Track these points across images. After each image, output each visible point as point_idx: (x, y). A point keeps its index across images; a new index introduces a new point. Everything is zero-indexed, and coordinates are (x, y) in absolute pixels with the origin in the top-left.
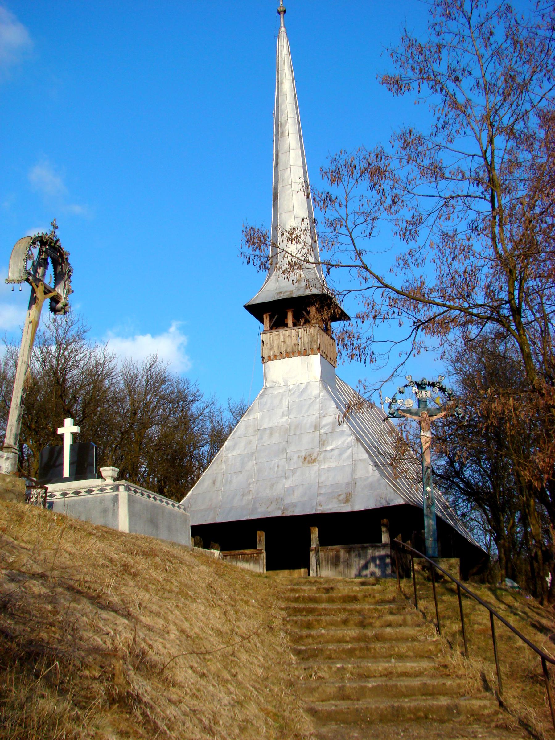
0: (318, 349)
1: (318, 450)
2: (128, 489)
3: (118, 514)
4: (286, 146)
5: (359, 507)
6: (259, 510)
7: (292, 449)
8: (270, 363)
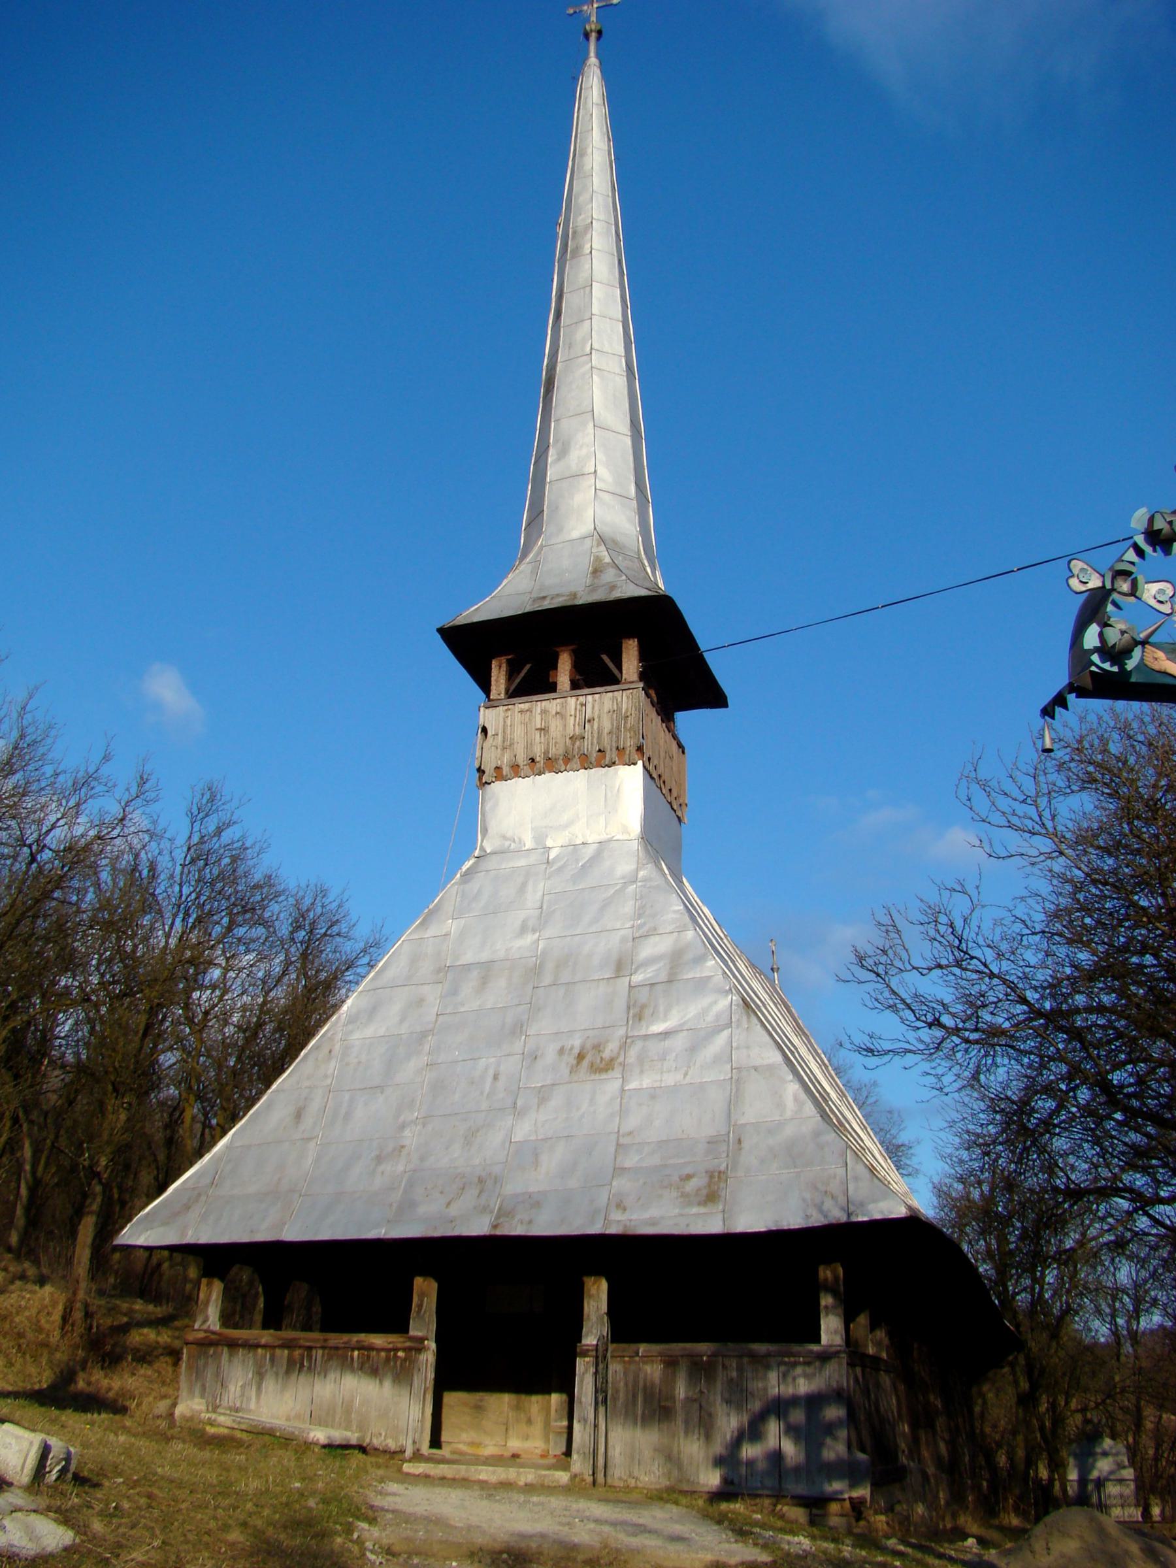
0: (640, 749)
4: (584, 275)
6: (422, 1210)
7: (543, 1026)
8: (498, 787)
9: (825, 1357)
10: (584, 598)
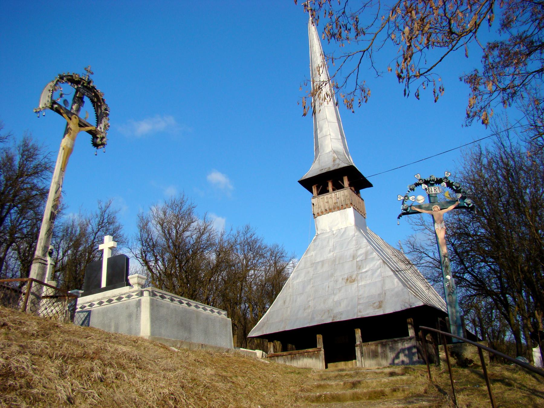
1: (356, 272)
2: (153, 294)
3: (140, 318)
5: (389, 310)
6: (316, 319)
8: (319, 218)
9: (411, 339)
10: (332, 169)
